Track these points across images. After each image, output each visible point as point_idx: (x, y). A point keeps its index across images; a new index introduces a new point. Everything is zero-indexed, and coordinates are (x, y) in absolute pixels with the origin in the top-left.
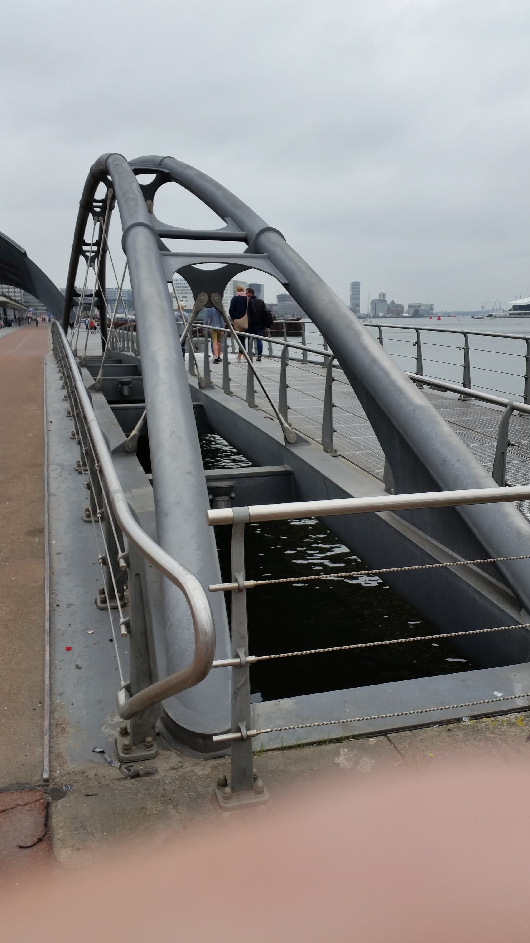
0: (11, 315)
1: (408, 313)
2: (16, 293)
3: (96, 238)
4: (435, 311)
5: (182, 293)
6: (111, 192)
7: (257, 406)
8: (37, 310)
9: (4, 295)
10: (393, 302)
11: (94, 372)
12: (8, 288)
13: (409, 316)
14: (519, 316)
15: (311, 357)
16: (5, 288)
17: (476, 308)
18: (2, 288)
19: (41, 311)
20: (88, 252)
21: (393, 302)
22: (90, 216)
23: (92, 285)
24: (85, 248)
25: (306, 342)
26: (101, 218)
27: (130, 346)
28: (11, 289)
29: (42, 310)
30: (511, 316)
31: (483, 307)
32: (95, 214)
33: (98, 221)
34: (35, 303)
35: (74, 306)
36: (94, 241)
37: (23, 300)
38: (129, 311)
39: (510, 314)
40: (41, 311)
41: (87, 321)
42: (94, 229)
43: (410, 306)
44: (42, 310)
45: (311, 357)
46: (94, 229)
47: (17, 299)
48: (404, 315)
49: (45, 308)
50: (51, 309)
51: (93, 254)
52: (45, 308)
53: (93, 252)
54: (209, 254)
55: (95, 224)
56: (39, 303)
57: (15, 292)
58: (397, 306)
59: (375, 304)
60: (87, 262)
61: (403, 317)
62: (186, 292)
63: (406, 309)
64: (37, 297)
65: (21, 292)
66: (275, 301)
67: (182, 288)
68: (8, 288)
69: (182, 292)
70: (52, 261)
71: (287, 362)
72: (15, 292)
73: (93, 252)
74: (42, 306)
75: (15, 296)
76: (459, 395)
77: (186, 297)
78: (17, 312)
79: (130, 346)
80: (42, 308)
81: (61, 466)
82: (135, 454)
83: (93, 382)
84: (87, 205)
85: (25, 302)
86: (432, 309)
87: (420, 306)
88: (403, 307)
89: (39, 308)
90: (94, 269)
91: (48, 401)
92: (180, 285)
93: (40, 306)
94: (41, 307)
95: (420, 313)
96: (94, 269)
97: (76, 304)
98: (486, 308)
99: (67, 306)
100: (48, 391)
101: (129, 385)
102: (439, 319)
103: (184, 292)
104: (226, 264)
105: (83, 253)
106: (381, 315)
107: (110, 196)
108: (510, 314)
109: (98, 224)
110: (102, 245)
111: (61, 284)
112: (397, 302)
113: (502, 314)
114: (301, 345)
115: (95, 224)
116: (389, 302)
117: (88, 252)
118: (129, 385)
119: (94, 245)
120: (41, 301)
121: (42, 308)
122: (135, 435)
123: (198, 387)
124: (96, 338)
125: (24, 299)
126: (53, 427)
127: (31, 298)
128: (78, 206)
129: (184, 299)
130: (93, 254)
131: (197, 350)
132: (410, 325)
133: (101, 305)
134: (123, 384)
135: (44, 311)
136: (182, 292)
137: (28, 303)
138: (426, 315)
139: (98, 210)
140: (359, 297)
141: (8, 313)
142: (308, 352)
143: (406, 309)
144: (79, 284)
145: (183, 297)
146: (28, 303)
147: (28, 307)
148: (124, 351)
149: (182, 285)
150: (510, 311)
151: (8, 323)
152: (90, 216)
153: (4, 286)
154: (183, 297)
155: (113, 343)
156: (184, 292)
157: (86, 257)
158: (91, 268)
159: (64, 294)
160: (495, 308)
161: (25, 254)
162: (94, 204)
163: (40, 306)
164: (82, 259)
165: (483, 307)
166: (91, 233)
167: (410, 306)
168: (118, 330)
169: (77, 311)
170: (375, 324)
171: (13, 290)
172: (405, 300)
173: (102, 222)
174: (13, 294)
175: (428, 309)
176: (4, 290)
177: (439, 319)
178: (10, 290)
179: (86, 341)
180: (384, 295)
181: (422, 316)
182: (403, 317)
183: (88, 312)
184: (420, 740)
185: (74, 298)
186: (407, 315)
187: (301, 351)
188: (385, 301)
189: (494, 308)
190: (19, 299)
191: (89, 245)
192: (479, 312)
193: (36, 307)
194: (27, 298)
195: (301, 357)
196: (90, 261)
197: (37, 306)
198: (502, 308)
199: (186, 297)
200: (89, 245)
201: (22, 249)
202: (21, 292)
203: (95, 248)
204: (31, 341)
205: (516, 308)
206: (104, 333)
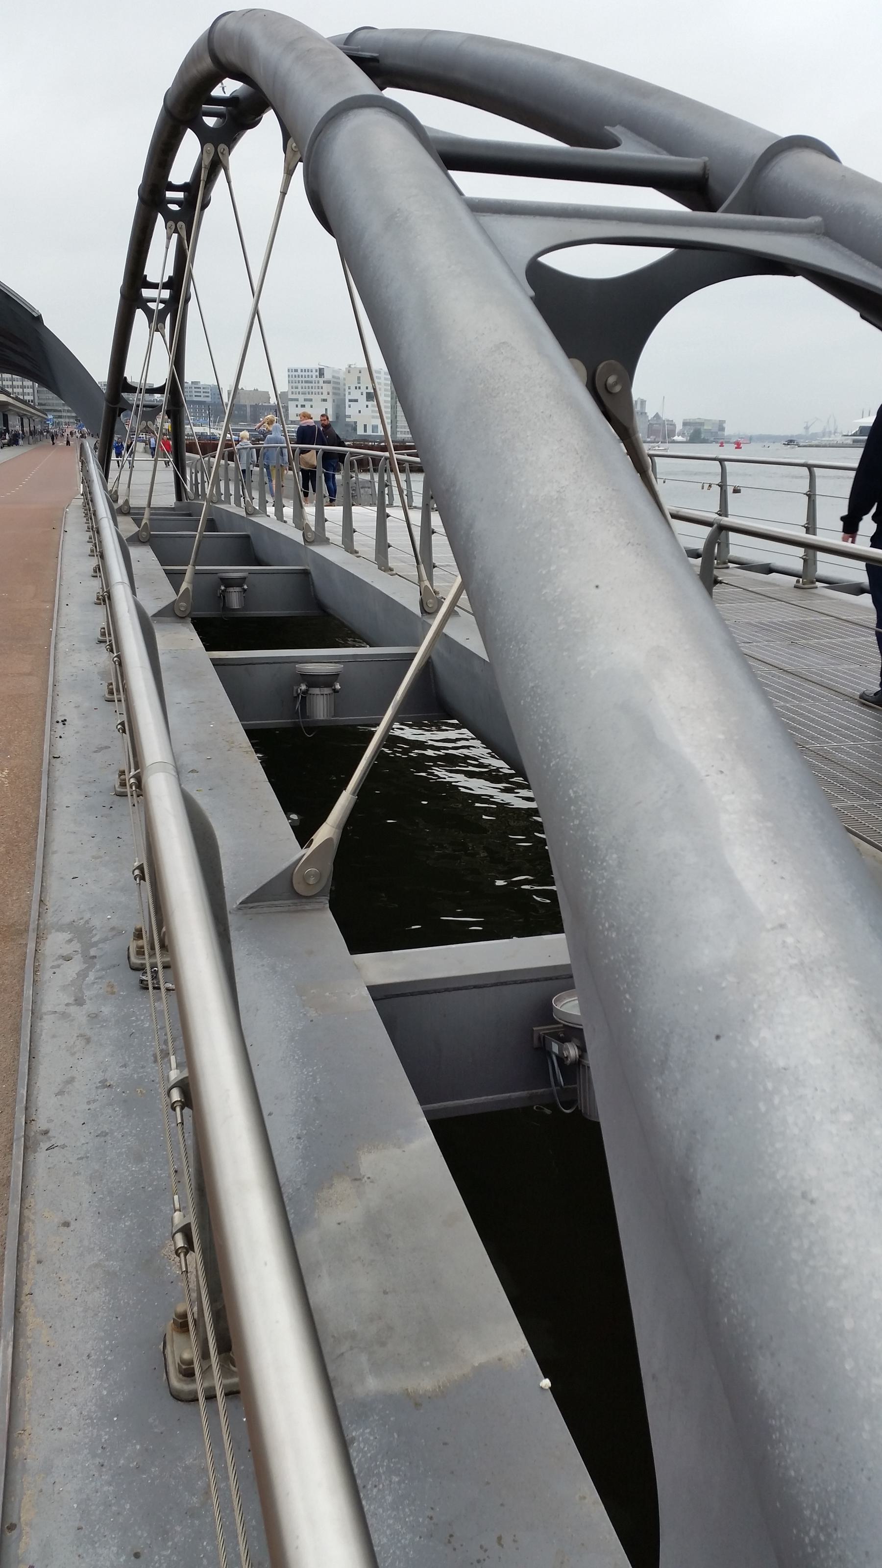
0: (15, 424)
1: (683, 435)
2: (20, 388)
3: (170, 272)
4: (727, 433)
5: (304, 393)
6: (208, 153)
7: (391, 570)
8: (60, 417)
9: (3, 392)
11: (169, 556)
12: (12, 380)
13: (684, 439)
15: (827, 566)
16: (7, 379)
18: (2, 380)
19: (67, 420)
20: (154, 300)
21: (657, 416)
22: (160, 219)
23: (160, 375)
24: (146, 293)
25: (819, 524)
26: (181, 224)
27: (232, 492)
28: (18, 380)
29: (69, 417)
31: (807, 428)
32: (169, 217)
33: (176, 231)
34: (57, 405)
35: (122, 410)
36: (166, 279)
37: (37, 401)
38: (215, 422)
39: (854, 441)
40: (67, 420)
41: (153, 440)
42: (167, 248)
43: (685, 424)
44: (69, 417)
45: (827, 566)
46: (167, 248)
47: (27, 398)
48: (676, 438)
49: (74, 414)
50: (83, 417)
51: (161, 306)
52: (74, 414)
53: (162, 301)
54: (625, 210)
55: (169, 238)
56: (64, 405)
57: (23, 387)
60: (150, 321)
61: (674, 442)
62: (310, 390)
63: (679, 427)
64: (60, 396)
65: (33, 387)
67: (304, 385)
68: (12, 380)
69: (304, 390)
71: (716, 572)
72: (23, 387)
73: (162, 301)
74: (68, 411)
75: (24, 394)
76: (794, 579)
77: (311, 400)
78: (26, 421)
79: (232, 492)
80: (69, 414)
81: (81, 932)
82: (325, 900)
83: (173, 597)
84: (153, 195)
85: (40, 404)
86: (722, 429)
87: (702, 424)
88: (674, 425)
89: (64, 414)
90: (163, 337)
91: (61, 645)
92: (300, 379)
93: (64, 411)
94: (67, 413)
95: (703, 436)
96: (163, 337)
97: (126, 407)
98: (812, 430)
99: (110, 411)
100: (65, 610)
101: (241, 586)
102: (722, 446)
103: (307, 390)
104: (662, 253)
105: (143, 303)
107: (207, 162)
108: (854, 441)
109: (175, 236)
110: (178, 283)
111: (99, 372)
112: (665, 416)
113: (839, 439)
114: (800, 534)
115: (169, 238)
117: (154, 300)
118: (241, 586)
119: (165, 286)
120: (67, 403)
121: (69, 414)
122: (328, 841)
123: (417, 610)
124: (166, 475)
125: (39, 399)
126: (68, 743)
127: (49, 397)
128: (135, 199)
129: (308, 404)
130: (161, 306)
132: (797, 458)
133: (175, 410)
134: (229, 583)
135: (72, 420)
136: (304, 390)
137: (44, 405)
138: (712, 439)
139: (174, 207)
141: (10, 423)
142: (820, 555)
143: (679, 427)
144: (132, 374)
145: (305, 400)
146: (44, 405)
147: (44, 412)
148: (220, 501)
149: (304, 379)
150: (854, 435)
151: (14, 441)
152: (160, 219)
153: (5, 376)
154: (305, 400)
155: (197, 483)
156: (307, 390)
157: (149, 313)
158: (157, 335)
159: (104, 389)
160: (827, 430)
161: (39, 319)
162: (169, 194)
163: (64, 411)
164: (140, 316)
165: (807, 428)
166: (158, 265)
167: (685, 424)
168: (207, 459)
169: (129, 421)
170: (714, 456)
171: (20, 383)
173: (184, 234)
174: (20, 390)
175: (715, 429)
176: (4, 383)
177: (722, 446)
178: (10, 383)
179: (147, 479)
181: (704, 441)
182: (674, 442)
183: (150, 423)
185: (125, 395)
186: (680, 438)
187: (801, 551)
189: (825, 429)
190: (31, 398)
191: (154, 286)
193: (60, 413)
194: (43, 396)
195: (798, 565)
196: (156, 320)
197: (60, 411)
198: (839, 431)
199: (311, 400)
200: (154, 286)
201: (33, 309)
202: (33, 387)
203: (166, 294)
204: (44, 475)
206: (180, 464)
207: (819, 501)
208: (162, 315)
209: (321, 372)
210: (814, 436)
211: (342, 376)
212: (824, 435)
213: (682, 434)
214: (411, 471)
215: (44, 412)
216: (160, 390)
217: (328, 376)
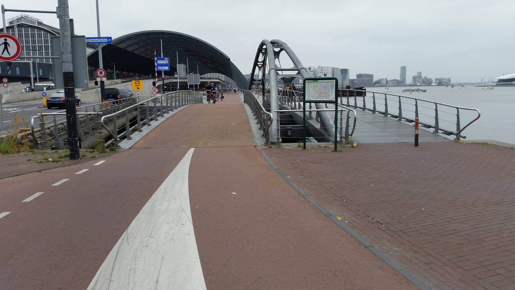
10: (426, 77)
14: (503, 85)
17: (479, 81)
21: (426, 77)
23: (260, 77)
28: (220, 75)
30: (497, 85)
31: (482, 80)
32: (263, 53)
43: (436, 80)
58: (428, 79)
59: (414, 78)
63: (434, 81)
64: (232, 79)
66: (355, 78)
70: (245, 68)
86: (450, 81)
87: (442, 80)
98: (484, 81)
99: (248, 84)
102: (452, 87)
105: (258, 65)
106: (418, 84)
110: (264, 62)
112: (428, 77)
116: (423, 77)
127: (229, 80)
131: (301, 101)
139: (264, 51)
140: (405, 75)
143: (434, 81)
147: (228, 84)
157: (259, 67)
164: (257, 67)
165: (482, 80)
166: (261, 59)
167: (436, 80)
172: (433, 76)
175: (447, 81)
177: (452, 87)
180: (420, 73)
184: (294, 123)
188: (421, 77)
192: (479, 83)
193: (232, 84)
205: (500, 81)
206: (264, 95)
207: (418, 107)
208: (261, 67)
209: (310, 69)
210: (485, 83)
211: (316, 69)
212: (489, 82)
213: (435, 83)
214: (343, 96)
215: (228, 84)
216: (260, 80)
217: (312, 69)
